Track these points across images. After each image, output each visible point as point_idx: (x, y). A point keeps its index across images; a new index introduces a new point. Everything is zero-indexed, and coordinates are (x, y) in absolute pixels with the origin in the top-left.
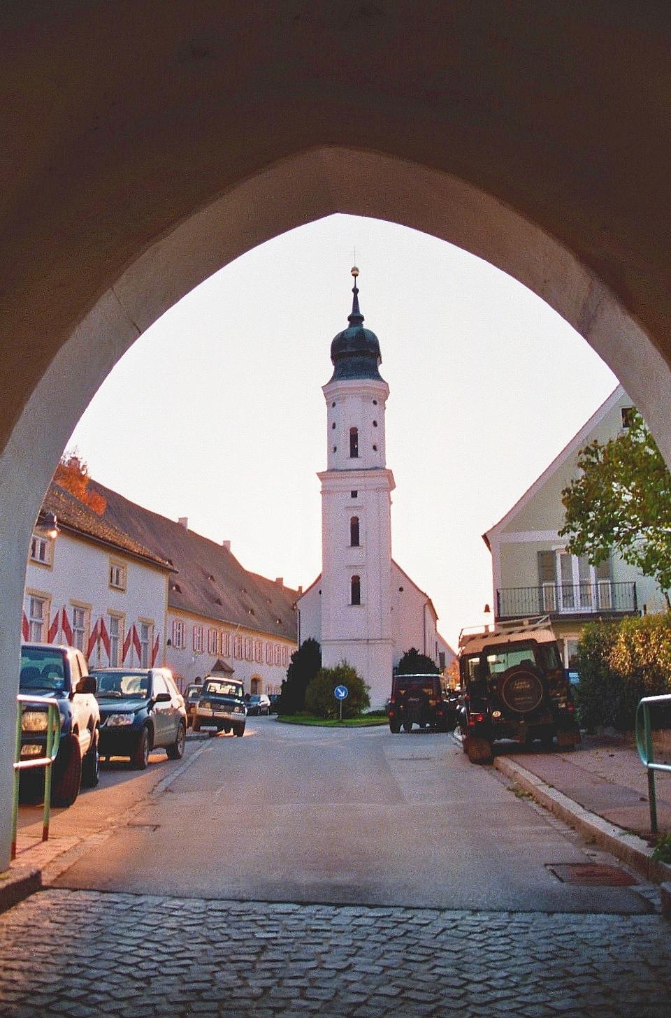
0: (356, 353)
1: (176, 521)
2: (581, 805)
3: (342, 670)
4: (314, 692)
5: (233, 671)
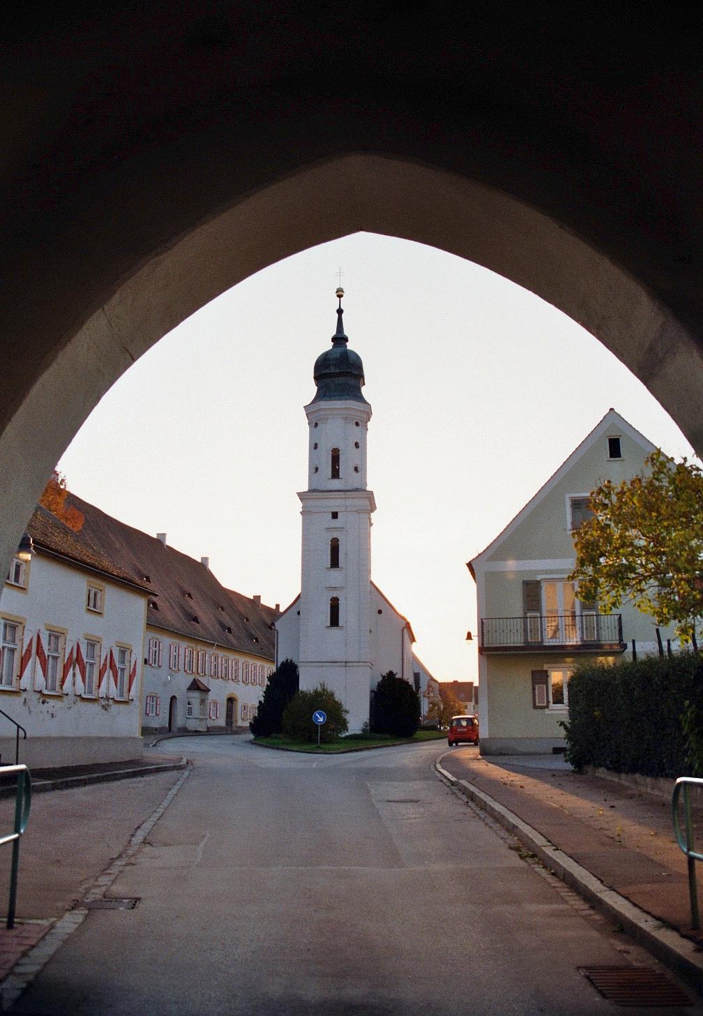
0: (339, 374)
1: (155, 536)
2: (600, 879)
3: (320, 693)
4: (290, 716)
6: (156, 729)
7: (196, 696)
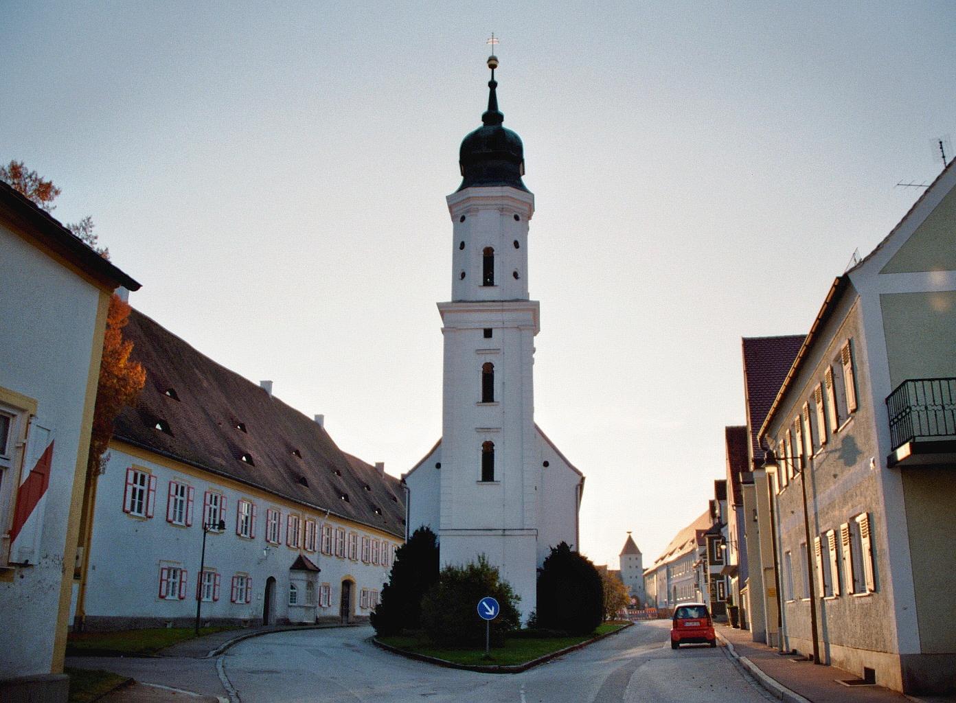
0: (492, 157)
3: (477, 570)
5: (320, 571)
6: (245, 621)
7: (301, 578)
